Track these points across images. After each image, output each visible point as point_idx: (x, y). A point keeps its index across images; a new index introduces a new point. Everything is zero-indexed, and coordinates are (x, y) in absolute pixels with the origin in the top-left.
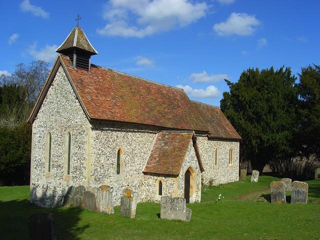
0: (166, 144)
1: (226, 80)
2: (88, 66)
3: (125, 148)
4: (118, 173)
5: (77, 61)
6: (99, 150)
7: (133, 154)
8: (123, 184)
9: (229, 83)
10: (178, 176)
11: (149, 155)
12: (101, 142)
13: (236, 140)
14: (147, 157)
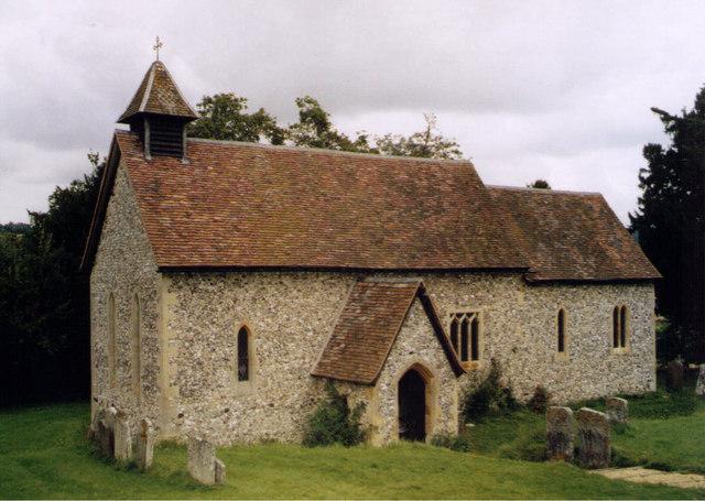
0: (364, 309)
1: (655, 110)
2: (182, 148)
3: (257, 324)
4: (244, 376)
5: (151, 140)
6: (190, 330)
7: (282, 337)
8: (259, 401)
9: (666, 117)
10: (373, 384)
11: (330, 336)
12: (192, 314)
13: (639, 282)
14: (324, 340)
